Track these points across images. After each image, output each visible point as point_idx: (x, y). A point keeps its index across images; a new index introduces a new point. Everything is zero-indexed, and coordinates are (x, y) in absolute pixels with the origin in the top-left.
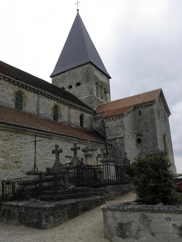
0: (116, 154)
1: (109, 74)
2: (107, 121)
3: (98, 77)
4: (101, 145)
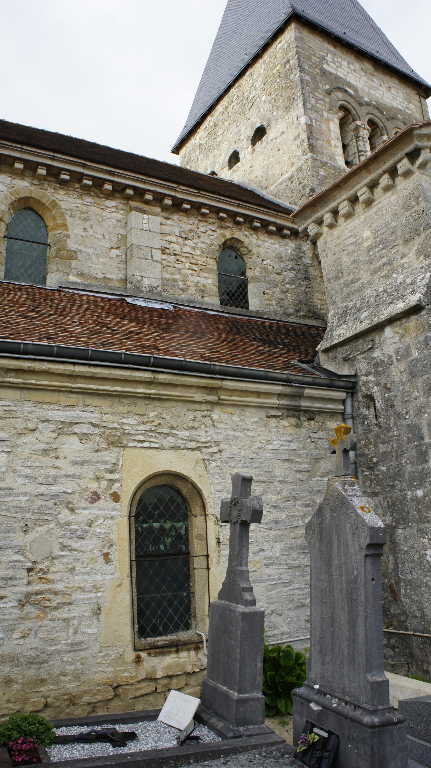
0: (382, 448)
1: (415, 74)
2: (325, 229)
3: (349, 85)
4: (228, 384)
